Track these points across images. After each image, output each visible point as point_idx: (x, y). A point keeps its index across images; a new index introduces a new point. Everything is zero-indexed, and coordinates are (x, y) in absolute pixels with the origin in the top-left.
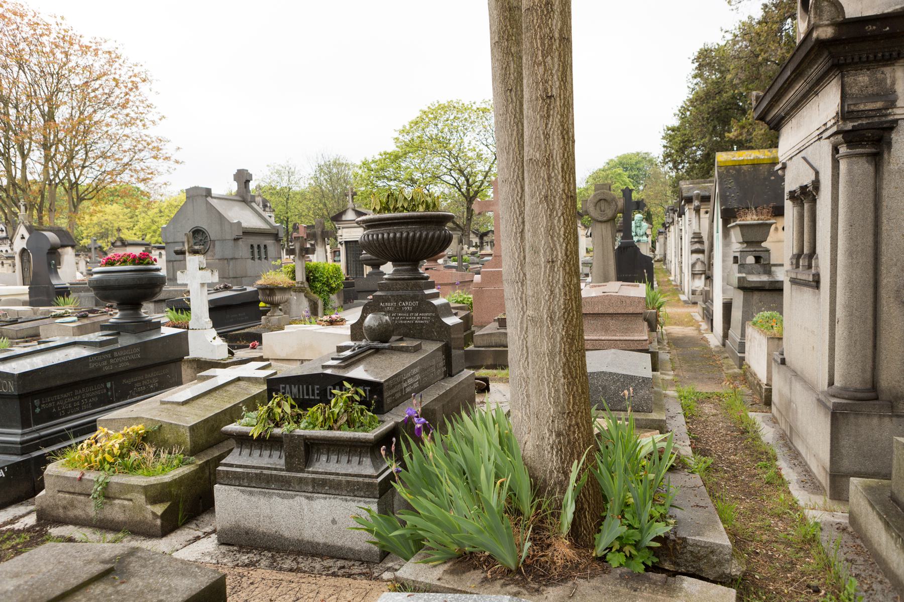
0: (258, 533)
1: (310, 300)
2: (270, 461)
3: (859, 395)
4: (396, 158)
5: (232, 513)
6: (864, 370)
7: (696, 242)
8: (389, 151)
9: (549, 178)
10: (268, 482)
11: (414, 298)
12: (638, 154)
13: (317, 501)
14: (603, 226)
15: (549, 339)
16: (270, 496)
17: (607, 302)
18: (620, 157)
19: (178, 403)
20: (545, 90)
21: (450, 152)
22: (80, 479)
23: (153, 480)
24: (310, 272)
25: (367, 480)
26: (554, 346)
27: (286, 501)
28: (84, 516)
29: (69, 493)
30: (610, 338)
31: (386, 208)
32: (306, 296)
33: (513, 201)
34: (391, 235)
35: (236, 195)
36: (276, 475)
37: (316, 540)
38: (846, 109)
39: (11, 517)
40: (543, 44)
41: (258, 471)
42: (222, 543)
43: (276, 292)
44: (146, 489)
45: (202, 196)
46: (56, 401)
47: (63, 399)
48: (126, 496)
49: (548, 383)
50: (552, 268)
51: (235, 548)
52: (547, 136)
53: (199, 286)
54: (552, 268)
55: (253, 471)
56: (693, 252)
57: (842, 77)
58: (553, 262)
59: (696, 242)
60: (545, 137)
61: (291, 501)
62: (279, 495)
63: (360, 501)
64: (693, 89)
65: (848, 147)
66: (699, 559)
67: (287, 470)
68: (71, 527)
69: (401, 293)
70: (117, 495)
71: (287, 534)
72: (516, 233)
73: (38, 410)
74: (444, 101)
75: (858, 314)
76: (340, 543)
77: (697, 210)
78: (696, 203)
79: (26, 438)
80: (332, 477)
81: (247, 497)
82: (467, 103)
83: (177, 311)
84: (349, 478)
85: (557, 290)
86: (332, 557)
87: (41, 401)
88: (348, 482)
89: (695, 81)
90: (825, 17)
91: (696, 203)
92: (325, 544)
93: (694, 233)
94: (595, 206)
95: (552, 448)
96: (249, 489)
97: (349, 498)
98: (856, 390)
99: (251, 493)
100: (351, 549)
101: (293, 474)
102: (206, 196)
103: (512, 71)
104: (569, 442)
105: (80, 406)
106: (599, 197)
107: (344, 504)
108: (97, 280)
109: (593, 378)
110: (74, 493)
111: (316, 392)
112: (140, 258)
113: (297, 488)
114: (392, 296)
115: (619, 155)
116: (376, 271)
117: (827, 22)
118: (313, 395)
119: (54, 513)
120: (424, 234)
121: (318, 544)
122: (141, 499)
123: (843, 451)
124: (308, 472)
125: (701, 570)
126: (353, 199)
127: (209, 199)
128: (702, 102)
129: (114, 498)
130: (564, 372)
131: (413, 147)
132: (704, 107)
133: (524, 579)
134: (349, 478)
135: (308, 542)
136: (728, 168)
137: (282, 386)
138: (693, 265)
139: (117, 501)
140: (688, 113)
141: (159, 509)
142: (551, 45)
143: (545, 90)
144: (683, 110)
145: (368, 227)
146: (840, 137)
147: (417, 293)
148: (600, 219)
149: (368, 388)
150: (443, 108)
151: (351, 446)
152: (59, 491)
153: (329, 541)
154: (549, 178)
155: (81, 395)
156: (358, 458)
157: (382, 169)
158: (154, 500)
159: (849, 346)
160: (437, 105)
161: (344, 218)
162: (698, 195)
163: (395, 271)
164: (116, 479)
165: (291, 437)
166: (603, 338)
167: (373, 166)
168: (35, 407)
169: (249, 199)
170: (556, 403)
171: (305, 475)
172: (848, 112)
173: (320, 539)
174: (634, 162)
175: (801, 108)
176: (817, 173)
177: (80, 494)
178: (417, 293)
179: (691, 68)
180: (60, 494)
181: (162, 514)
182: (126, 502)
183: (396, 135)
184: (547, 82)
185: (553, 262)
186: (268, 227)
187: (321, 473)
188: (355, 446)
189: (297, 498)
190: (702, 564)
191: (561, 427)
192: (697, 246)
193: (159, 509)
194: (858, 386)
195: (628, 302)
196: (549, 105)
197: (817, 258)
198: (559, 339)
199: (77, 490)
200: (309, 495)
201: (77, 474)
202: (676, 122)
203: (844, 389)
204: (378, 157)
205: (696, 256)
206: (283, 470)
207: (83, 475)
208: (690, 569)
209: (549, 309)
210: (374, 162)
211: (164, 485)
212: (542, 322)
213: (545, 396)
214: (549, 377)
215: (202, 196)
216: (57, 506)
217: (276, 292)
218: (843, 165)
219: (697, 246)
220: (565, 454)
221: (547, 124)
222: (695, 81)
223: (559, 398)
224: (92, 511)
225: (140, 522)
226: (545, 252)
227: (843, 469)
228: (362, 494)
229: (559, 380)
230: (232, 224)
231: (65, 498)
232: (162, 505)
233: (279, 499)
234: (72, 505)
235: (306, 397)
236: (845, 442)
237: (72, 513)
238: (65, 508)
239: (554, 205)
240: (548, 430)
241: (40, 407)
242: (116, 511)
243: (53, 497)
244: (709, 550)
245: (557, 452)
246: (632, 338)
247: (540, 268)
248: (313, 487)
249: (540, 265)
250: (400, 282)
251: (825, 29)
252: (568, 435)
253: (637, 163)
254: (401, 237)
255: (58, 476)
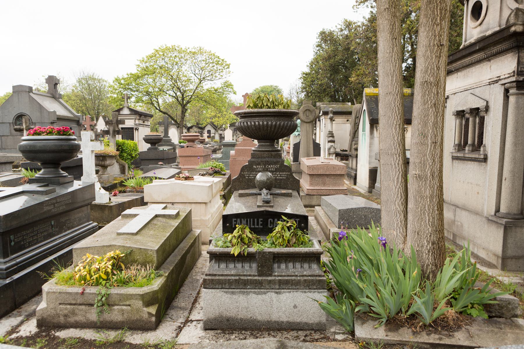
0: (237, 319)
1: (120, 165)
2: (250, 270)
3: (517, 217)
4: (136, 77)
5: (216, 308)
6: (518, 204)
7: (330, 136)
8: (133, 73)
9: (438, 93)
10: (245, 285)
11: (275, 163)
12: (272, 86)
13: (283, 295)
14: (308, 125)
15: (430, 188)
16: (248, 293)
17: (325, 168)
18: (262, 87)
19: (132, 234)
20: (440, 41)
21: (172, 77)
22: (83, 293)
23: (146, 289)
24: (119, 146)
25: (318, 278)
26: (433, 192)
27: (260, 296)
28: (85, 320)
29: (71, 304)
30: (327, 188)
31: (256, 106)
32: (117, 162)
33: (395, 106)
34: (265, 123)
35: (48, 93)
36: (251, 280)
37: (281, 320)
38: (520, 69)
39: (10, 329)
40: (441, 13)
41: (237, 278)
42: (206, 328)
43: (107, 158)
44: (142, 297)
45: (26, 92)
46: (23, 236)
47: (27, 234)
48: (125, 303)
49: (428, 214)
50: (435, 146)
51: (219, 331)
52: (438, 68)
53: (90, 152)
54: (435, 146)
55: (233, 278)
56: (329, 142)
57: (519, 53)
58: (436, 143)
59: (330, 136)
60: (437, 69)
61: (264, 296)
62: (255, 293)
63: (315, 292)
64: (317, 53)
65: (517, 90)
66: (502, 308)
67: (259, 276)
68: (72, 330)
69: (267, 159)
70: (117, 303)
71: (259, 318)
72: (396, 125)
73: (13, 243)
74: (169, 45)
75: (517, 175)
76: (299, 320)
77: (332, 119)
78: (331, 115)
79: (8, 265)
80: (293, 278)
81: (229, 296)
82: (183, 49)
83: (31, 170)
84: (305, 278)
85: (437, 160)
86: (293, 330)
87: (14, 237)
88: (305, 280)
89: (318, 49)
90: (520, 20)
91: (331, 115)
92: (287, 322)
93: (329, 132)
94: (304, 113)
95: (429, 252)
96: (230, 290)
97: (307, 291)
98: (515, 214)
99: (233, 293)
100: (306, 323)
101: (264, 278)
102: (29, 92)
103: (397, 27)
104: (439, 247)
105: (37, 239)
106: (306, 108)
107: (303, 295)
108: (25, 146)
109: (359, 211)
110: (75, 304)
111: (260, 223)
112: (64, 131)
113: (267, 287)
114: (262, 161)
115: (261, 86)
116: (153, 147)
117: (521, 23)
118: (258, 224)
119: (55, 321)
120: (278, 123)
121: (283, 322)
122: (139, 304)
123: (509, 246)
124: (275, 276)
125: (503, 314)
126: (127, 100)
127: (31, 94)
128: (326, 61)
129: (113, 305)
130: (437, 207)
131: (147, 72)
132: (327, 64)
133: (436, 329)
134: (305, 278)
135: (275, 322)
136: (371, 97)
137: (234, 220)
138: (329, 149)
139: (116, 307)
140: (314, 66)
141: (153, 310)
142: (445, 14)
143: (440, 41)
144: (312, 64)
145: (242, 117)
146: (514, 84)
147: (278, 160)
148: (306, 121)
149: (298, 220)
150: (168, 49)
151: (303, 257)
152: (60, 304)
153: (291, 320)
154: (438, 93)
155: (37, 230)
156: (285, 264)
157: (128, 84)
158: (148, 304)
159: (512, 192)
160: (165, 47)
161: (121, 113)
162: (332, 110)
163: (259, 146)
164: (115, 291)
165: (262, 254)
166: (323, 188)
167: (122, 82)
168: (11, 241)
169: (57, 96)
170: (433, 226)
171: (273, 278)
172: (520, 71)
173: (284, 319)
174: (269, 90)
175: (470, 67)
176: (487, 102)
177: (80, 304)
178: (278, 160)
179: (315, 40)
180: (61, 306)
181: (156, 313)
182: (124, 307)
183: (138, 63)
184: (441, 36)
185: (436, 143)
186: (72, 116)
187: (285, 276)
188: (305, 257)
189: (269, 293)
190: (504, 311)
191: (435, 239)
192: (331, 139)
193: (153, 310)
194: (516, 212)
195: (337, 168)
196: (441, 50)
197: (485, 146)
198: (436, 188)
199: (78, 302)
200: (278, 291)
201: (80, 290)
202: (307, 70)
203: (508, 214)
204: (126, 76)
205: (330, 144)
206: (256, 276)
207: (84, 290)
208: (497, 314)
209: (432, 170)
210: (123, 79)
211: (155, 293)
212: (426, 178)
213: (425, 221)
214: (430, 210)
215: (26, 92)
216: (58, 315)
217: (107, 158)
218: (512, 99)
219: (331, 139)
220: (437, 255)
221: (439, 61)
222: (318, 49)
223: (434, 222)
224: (93, 315)
225: (137, 320)
226: (431, 137)
227: (508, 255)
228: (315, 287)
229: (435, 212)
230: (49, 113)
231: (66, 309)
232: (153, 307)
233: (254, 296)
234: (73, 313)
235: (256, 227)
236: (510, 241)
237: (72, 320)
238: (66, 316)
239: (438, 109)
240: (427, 241)
241: (14, 241)
242: (115, 315)
243: (55, 309)
244: (508, 302)
245: (432, 254)
246: (339, 188)
247: (428, 146)
248: (280, 285)
249: (428, 145)
250: (266, 153)
251: (519, 26)
252: (438, 244)
253: (271, 92)
254: (272, 125)
255: (60, 293)
